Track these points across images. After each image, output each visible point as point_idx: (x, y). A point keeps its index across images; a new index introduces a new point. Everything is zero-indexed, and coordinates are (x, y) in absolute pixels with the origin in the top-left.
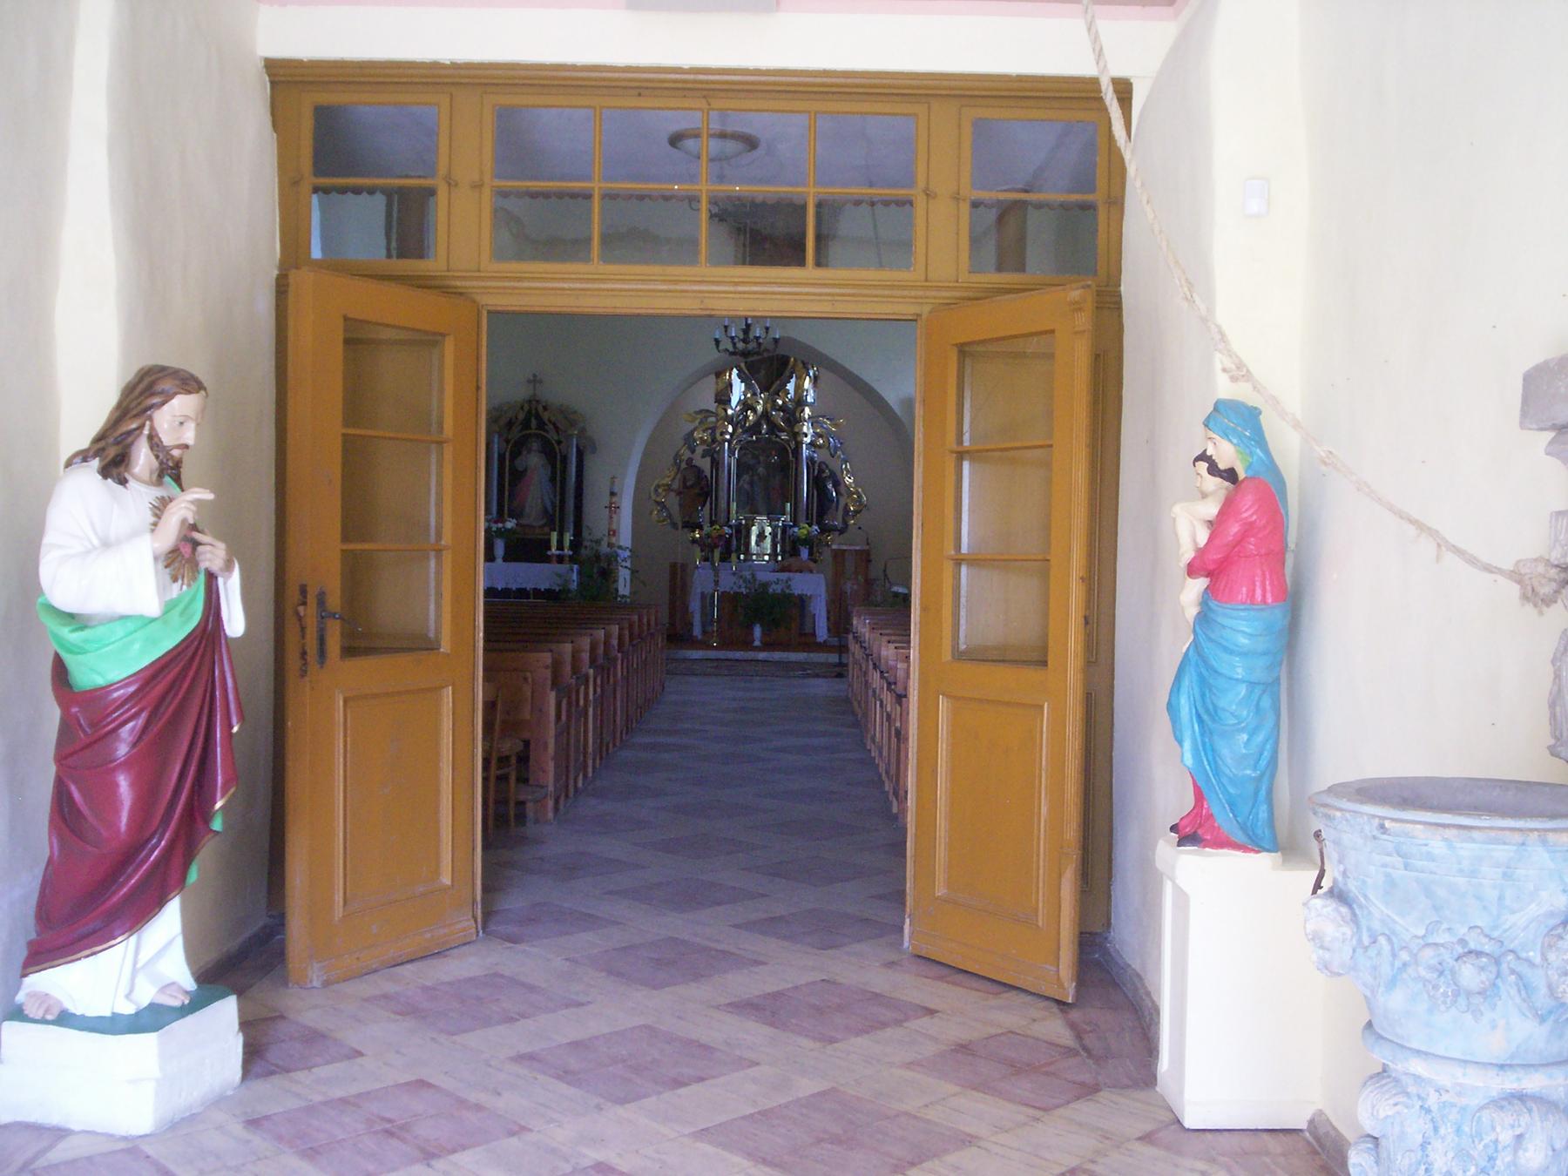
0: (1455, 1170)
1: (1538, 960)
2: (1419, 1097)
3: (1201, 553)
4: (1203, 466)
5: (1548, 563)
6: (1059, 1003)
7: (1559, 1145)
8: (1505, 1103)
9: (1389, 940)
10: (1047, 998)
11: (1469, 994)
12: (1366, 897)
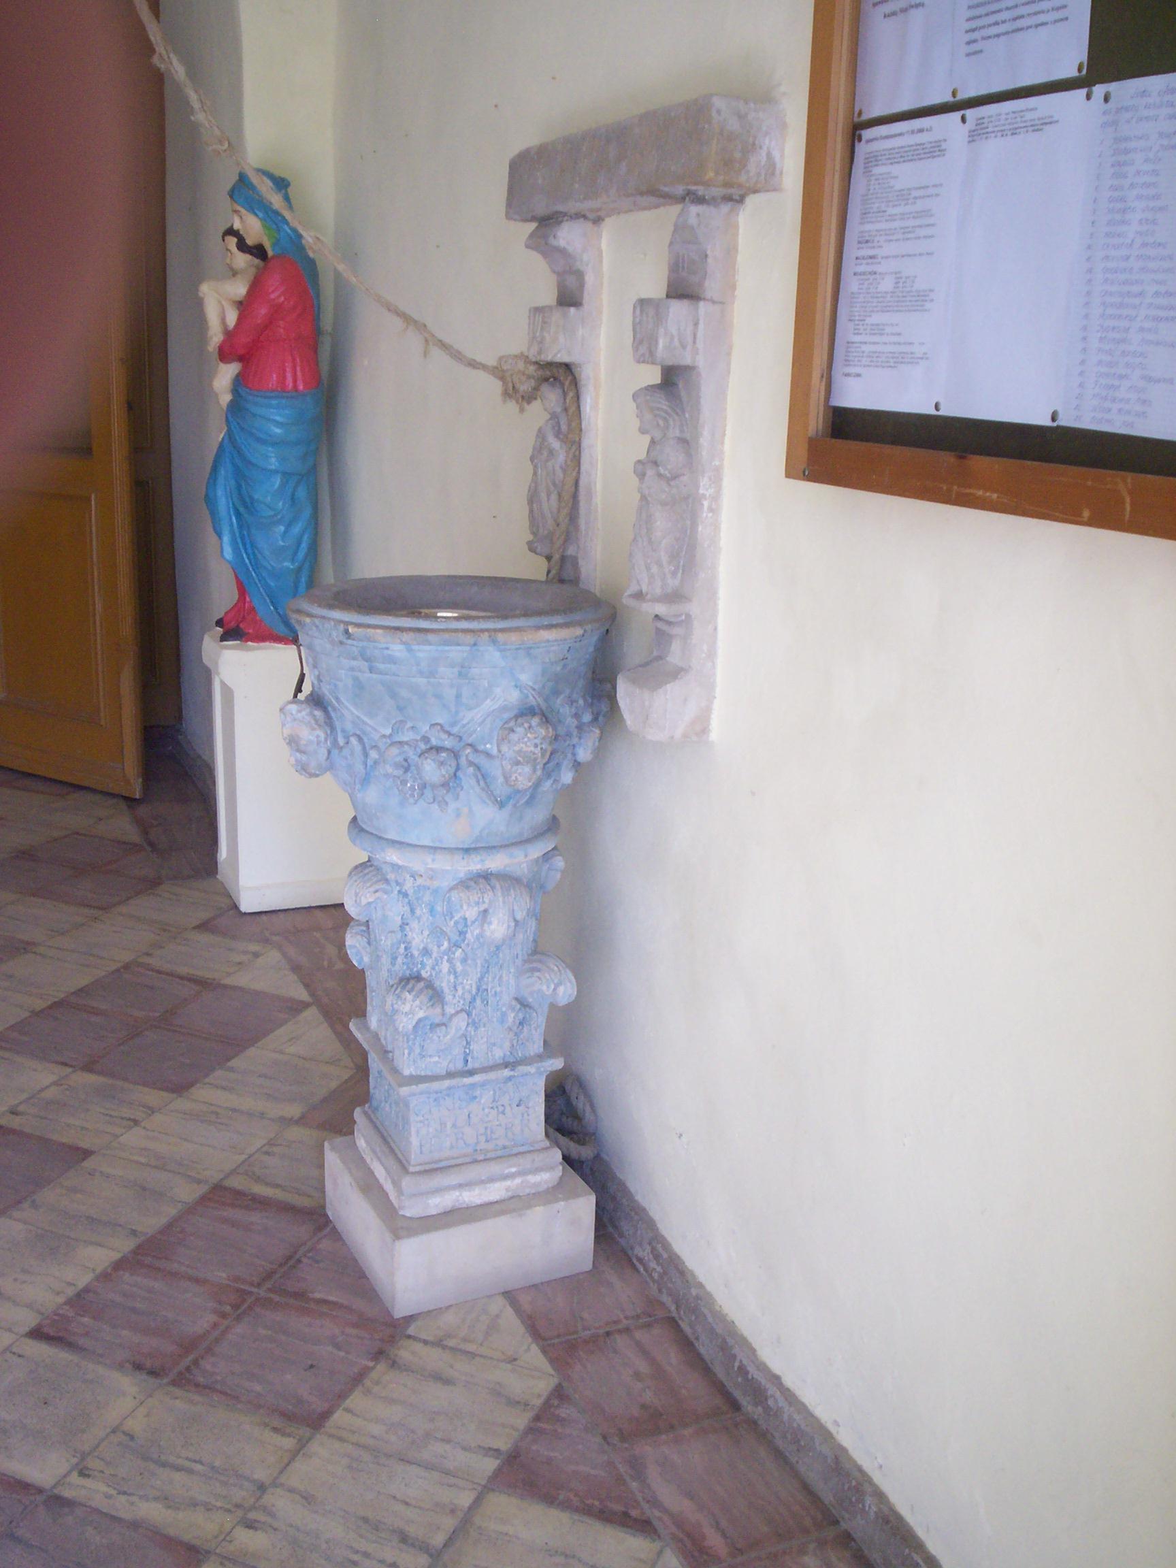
0: (430, 946)
1: (495, 752)
2: (397, 883)
3: (229, 335)
4: (232, 242)
5: (526, 359)
6: (126, 799)
7: (519, 916)
8: (472, 883)
9: (360, 739)
10: (113, 795)
11: (434, 787)
12: (337, 699)
